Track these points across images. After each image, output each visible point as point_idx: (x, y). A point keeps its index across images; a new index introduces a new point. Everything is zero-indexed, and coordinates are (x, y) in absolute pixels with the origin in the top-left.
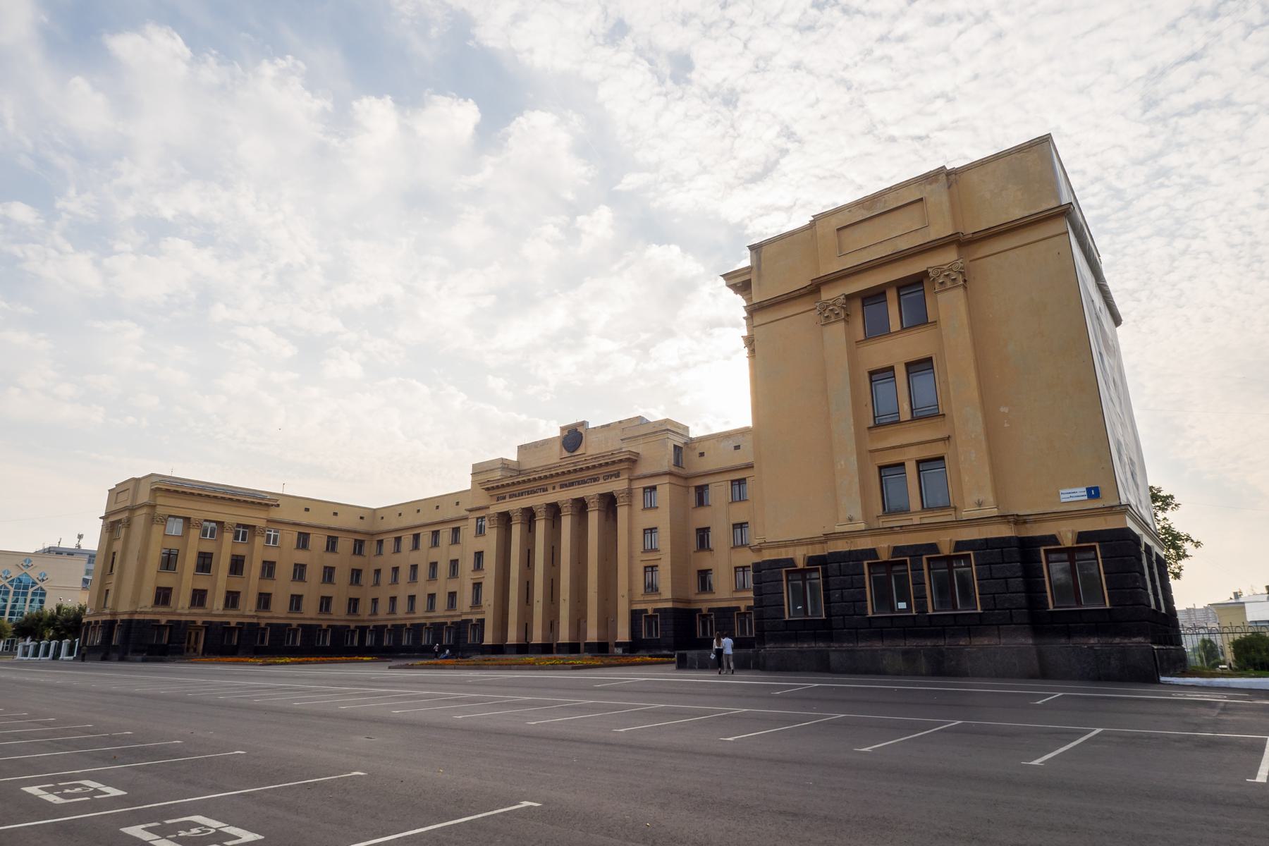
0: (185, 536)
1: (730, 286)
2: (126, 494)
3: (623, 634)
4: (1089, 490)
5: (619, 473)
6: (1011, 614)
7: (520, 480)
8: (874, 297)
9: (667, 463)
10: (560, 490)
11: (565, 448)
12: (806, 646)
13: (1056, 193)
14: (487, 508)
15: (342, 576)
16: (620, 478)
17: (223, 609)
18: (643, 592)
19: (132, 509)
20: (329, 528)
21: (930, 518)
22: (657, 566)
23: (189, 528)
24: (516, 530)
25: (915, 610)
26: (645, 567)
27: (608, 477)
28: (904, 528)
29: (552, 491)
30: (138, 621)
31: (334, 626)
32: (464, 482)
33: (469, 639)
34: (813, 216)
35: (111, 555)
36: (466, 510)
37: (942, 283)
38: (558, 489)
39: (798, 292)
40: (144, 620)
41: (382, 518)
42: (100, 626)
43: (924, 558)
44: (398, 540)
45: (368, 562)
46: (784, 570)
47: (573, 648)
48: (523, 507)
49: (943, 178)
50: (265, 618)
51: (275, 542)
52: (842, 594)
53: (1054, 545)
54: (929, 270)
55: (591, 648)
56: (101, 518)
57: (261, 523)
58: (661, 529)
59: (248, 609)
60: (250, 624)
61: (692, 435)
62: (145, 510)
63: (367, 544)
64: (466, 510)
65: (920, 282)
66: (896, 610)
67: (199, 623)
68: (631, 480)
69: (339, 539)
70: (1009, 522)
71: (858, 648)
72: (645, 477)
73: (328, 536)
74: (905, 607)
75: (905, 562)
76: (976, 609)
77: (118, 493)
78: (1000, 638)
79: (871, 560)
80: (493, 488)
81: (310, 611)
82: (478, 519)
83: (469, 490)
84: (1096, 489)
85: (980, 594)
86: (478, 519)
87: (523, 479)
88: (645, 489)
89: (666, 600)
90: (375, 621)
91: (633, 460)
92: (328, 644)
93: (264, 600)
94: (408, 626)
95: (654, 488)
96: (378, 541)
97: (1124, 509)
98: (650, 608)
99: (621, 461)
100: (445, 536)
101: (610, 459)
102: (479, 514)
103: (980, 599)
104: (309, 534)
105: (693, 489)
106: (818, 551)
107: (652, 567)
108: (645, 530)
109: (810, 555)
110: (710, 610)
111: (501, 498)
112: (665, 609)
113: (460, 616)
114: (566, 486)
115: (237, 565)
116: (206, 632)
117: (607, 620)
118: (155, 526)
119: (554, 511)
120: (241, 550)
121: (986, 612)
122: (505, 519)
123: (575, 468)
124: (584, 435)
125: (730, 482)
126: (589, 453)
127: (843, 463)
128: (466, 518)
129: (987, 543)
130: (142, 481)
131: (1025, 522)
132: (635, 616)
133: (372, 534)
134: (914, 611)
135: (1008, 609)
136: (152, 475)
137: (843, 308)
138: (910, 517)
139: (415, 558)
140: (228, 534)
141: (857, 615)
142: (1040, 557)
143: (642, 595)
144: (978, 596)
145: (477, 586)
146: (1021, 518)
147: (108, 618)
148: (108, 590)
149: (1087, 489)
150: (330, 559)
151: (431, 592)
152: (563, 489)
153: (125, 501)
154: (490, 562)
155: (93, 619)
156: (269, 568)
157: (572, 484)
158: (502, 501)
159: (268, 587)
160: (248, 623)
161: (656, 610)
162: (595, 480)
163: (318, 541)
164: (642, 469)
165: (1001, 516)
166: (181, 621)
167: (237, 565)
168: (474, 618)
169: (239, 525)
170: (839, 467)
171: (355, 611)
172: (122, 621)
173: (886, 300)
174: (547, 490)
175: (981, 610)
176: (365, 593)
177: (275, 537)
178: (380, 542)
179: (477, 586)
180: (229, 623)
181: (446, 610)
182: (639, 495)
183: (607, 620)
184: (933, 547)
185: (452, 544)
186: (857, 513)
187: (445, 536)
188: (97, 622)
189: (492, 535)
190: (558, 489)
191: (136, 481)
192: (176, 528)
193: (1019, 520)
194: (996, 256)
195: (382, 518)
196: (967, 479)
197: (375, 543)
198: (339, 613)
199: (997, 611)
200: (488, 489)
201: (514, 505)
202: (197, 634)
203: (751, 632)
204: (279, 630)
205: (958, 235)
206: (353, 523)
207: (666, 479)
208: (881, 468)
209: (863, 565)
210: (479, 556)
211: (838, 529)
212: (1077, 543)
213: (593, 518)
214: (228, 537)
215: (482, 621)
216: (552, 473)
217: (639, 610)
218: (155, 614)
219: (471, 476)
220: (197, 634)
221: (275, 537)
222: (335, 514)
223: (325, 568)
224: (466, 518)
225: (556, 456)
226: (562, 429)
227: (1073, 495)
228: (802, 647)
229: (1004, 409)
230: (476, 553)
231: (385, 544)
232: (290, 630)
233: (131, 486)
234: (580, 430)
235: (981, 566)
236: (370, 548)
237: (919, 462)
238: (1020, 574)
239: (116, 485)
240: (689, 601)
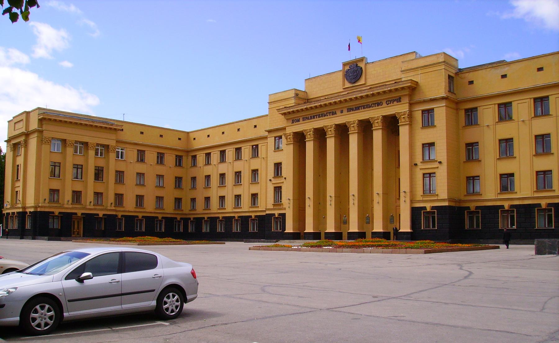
0: (64, 153)
2: (21, 123)
3: (405, 227)
5: (400, 98)
9: (441, 91)
15: (170, 182)
19: (27, 135)
24: (310, 146)
26: (424, 174)
27: (390, 102)
29: (340, 114)
32: (264, 110)
33: (466, 226)
36: (266, 131)
38: (345, 112)
41: (194, 139)
45: (185, 173)
47: (316, 236)
48: (359, 119)
55: (352, 236)
56: (5, 141)
57: (112, 143)
61: (461, 66)
62: (36, 135)
63: (184, 159)
64: (266, 131)
67: (101, 216)
68: (411, 105)
72: (425, 102)
77: (15, 123)
81: (150, 207)
89: (444, 200)
90: (256, 211)
92: (208, 230)
94: (253, 217)
99: (403, 88)
100: (246, 151)
104: (144, 151)
105: (463, 112)
107: (430, 174)
108: (423, 144)
110: (477, 208)
111: (295, 121)
113: (265, 211)
114: (352, 110)
115: (99, 174)
118: (43, 146)
120: (101, 163)
125: (497, 106)
126: (370, 82)
128: (266, 138)
130: (31, 114)
132: (415, 212)
133: (188, 152)
139: (223, 168)
143: (421, 196)
145: (278, 190)
147: (21, 210)
148: (17, 192)
150: (160, 169)
151: (238, 194)
152: (350, 113)
153: (21, 128)
154: (288, 170)
155: (10, 211)
158: (297, 123)
159: (121, 190)
161: (433, 208)
162: (379, 104)
167: (99, 174)
168: (276, 213)
169: (98, 145)
171: (179, 207)
172: (30, 212)
174: (335, 113)
176: (186, 195)
178: (194, 157)
179: (278, 190)
180: (98, 215)
182: (418, 116)
187: (246, 151)
188: (13, 213)
190: (345, 112)
191: (27, 113)
192: (56, 147)
197: (190, 158)
198: (169, 208)
200: (284, 114)
201: (308, 126)
203: (478, 226)
204: (130, 219)
207: (443, 103)
210: (278, 166)
213: (378, 136)
214: (92, 153)
215: (283, 216)
218: (50, 207)
222: (161, 136)
224: (266, 138)
226: (344, 65)
232: (176, 222)
233: (24, 117)
234: (362, 65)
236: (187, 161)
240: (460, 201)
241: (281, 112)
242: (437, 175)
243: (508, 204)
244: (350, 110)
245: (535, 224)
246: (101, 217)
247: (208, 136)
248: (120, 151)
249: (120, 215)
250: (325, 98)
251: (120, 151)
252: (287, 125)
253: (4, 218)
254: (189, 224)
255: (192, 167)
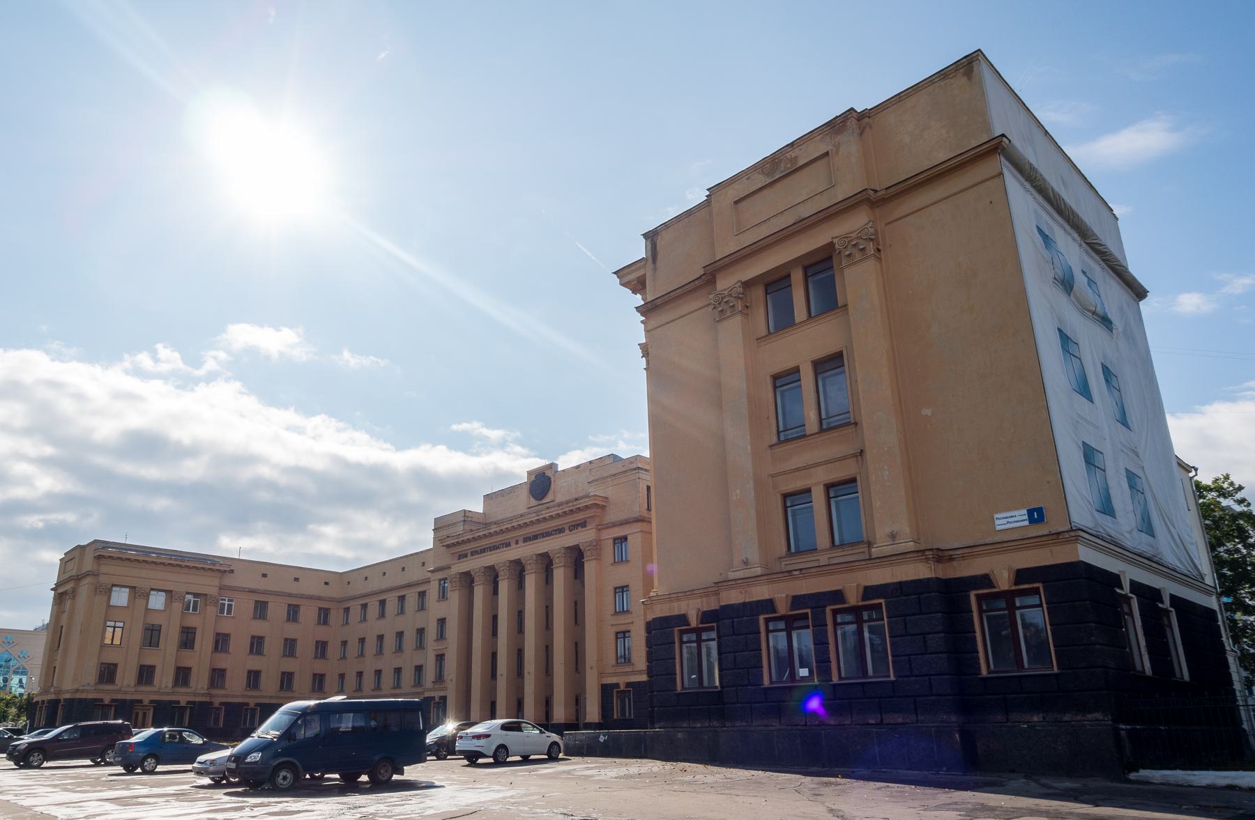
1: (624, 284)
3: (593, 712)
4: (1030, 512)
5: (586, 522)
6: (930, 683)
7: (480, 534)
8: (776, 283)
10: (523, 545)
11: (533, 496)
12: (699, 725)
13: (987, 126)
14: (449, 568)
15: (273, 647)
16: (588, 528)
17: (173, 687)
18: (614, 662)
19: (78, 579)
20: (290, 595)
21: (839, 556)
22: (629, 631)
23: (135, 598)
25: (817, 677)
26: (617, 633)
27: (574, 527)
28: (804, 572)
30: (80, 700)
31: (229, 703)
32: (426, 541)
33: (432, 720)
34: (708, 190)
35: (60, 628)
37: (849, 255)
38: (521, 543)
39: (693, 284)
40: (86, 699)
42: (62, 705)
43: (828, 610)
44: (364, 606)
45: (333, 633)
46: (677, 628)
49: (852, 123)
50: (219, 697)
51: (229, 612)
52: (735, 658)
53: (987, 588)
54: (835, 241)
56: (52, 589)
57: (213, 591)
58: (633, 588)
59: (199, 685)
60: (202, 704)
65: (830, 258)
66: (797, 678)
67: (183, 704)
69: (302, 608)
70: (928, 559)
71: (752, 729)
72: (614, 525)
73: (256, 601)
74: (807, 675)
75: (805, 617)
76: (889, 676)
78: (917, 715)
79: (767, 613)
80: (454, 545)
82: (440, 580)
83: (430, 549)
84: (1040, 510)
85: (893, 656)
86: (440, 580)
87: (484, 533)
88: (615, 539)
89: (640, 672)
91: (601, 506)
93: (218, 676)
95: (625, 538)
96: (345, 609)
97: (1073, 534)
98: (622, 681)
101: (574, 506)
102: (440, 575)
103: (893, 662)
104: (267, 602)
106: (712, 604)
107: (624, 633)
109: (705, 609)
111: (462, 556)
112: (639, 682)
116: (154, 712)
117: (578, 701)
119: (518, 569)
121: (901, 679)
122: (467, 580)
123: (538, 518)
124: (552, 480)
126: (560, 499)
127: (738, 492)
129: (901, 589)
130: (87, 549)
131: (951, 559)
134: (816, 680)
135: (927, 675)
136: (96, 541)
137: (741, 298)
138: (817, 558)
140: (176, 604)
141: (752, 685)
142: (970, 605)
144: (890, 658)
145: (440, 658)
146: (946, 553)
147: (52, 697)
148: (55, 667)
149: (1028, 510)
152: (526, 544)
153: (73, 570)
156: (221, 642)
157: (483, 551)
158: (465, 559)
160: (199, 702)
161: (628, 685)
163: (277, 610)
164: (612, 516)
165: (918, 551)
166: (125, 700)
168: (437, 695)
170: (734, 498)
172: (65, 700)
173: (790, 285)
175: (895, 677)
177: (230, 606)
178: (347, 610)
179: (440, 658)
180: (178, 702)
181: (412, 686)
182: (608, 548)
183: (578, 701)
184: (838, 596)
185: (418, 610)
186: (753, 554)
189: (455, 597)
190: (521, 543)
191: (81, 548)
193: (941, 556)
194: (914, 214)
195: (349, 583)
196: (878, 504)
197: (341, 611)
199: (912, 678)
200: (448, 546)
201: (475, 564)
202: (145, 714)
203: (630, 715)
205: (865, 193)
206: (316, 589)
208: (786, 496)
209: (758, 621)
210: (442, 622)
211: (732, 575)
212: (1016, 584)
215: (444, 699)
216: (513, 525)
217: (610, 684)
219: (432, 532)
220: (145, 714)
221: (230, 606)
223: (286, 640)
224: (428, 581)
225: (523, 502)
227: (1012, 520)
228: (695, 728)
229: (927, 412)
230: (438, 620)
231: (352, 611)
232: (247, 710)
234: (549, 473)
235: (894, 619)
236: (335, 617)
237: (828, 487)
238: (941, 628)
239: (65, 554)
241: (445, 544)
242: (632, 634)
243: (784, 595)
244: (526, 540)
245: (826, 631)
246: (184, 707)
247: (366, 578)
248: (227, 603)
249: (217, 702)
250: (1008, 522)
251: (227, 603)
252: (453, 563)
253: (60, 707)
254: (615, 698)
255: (361, 621)
